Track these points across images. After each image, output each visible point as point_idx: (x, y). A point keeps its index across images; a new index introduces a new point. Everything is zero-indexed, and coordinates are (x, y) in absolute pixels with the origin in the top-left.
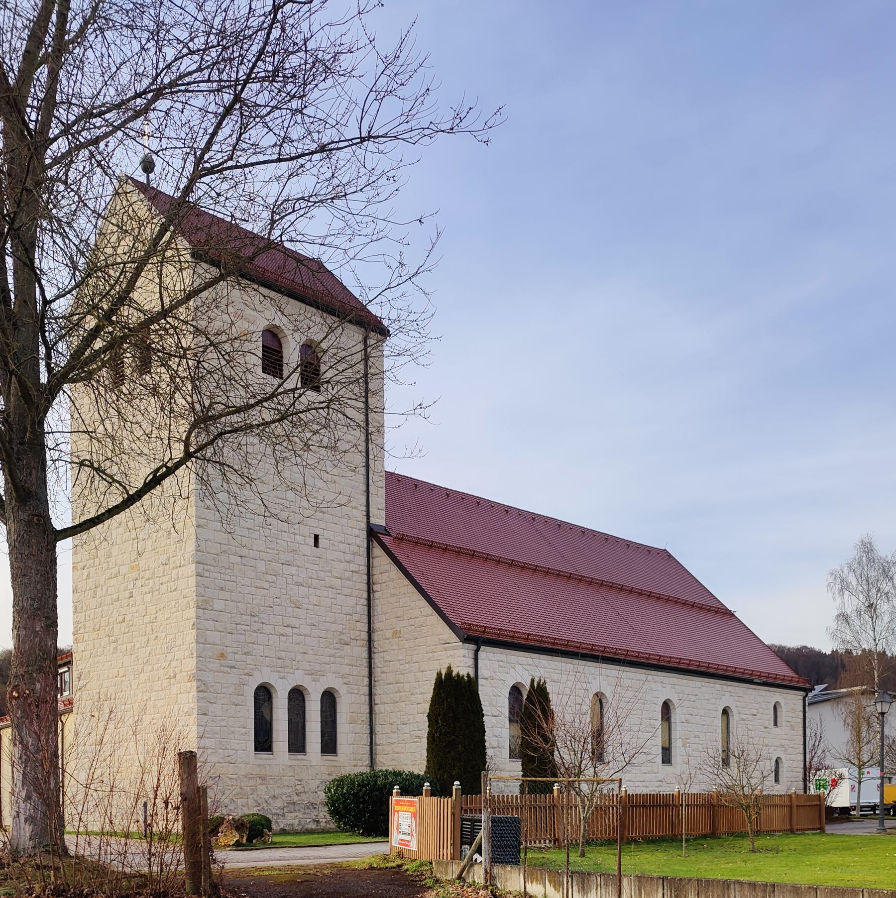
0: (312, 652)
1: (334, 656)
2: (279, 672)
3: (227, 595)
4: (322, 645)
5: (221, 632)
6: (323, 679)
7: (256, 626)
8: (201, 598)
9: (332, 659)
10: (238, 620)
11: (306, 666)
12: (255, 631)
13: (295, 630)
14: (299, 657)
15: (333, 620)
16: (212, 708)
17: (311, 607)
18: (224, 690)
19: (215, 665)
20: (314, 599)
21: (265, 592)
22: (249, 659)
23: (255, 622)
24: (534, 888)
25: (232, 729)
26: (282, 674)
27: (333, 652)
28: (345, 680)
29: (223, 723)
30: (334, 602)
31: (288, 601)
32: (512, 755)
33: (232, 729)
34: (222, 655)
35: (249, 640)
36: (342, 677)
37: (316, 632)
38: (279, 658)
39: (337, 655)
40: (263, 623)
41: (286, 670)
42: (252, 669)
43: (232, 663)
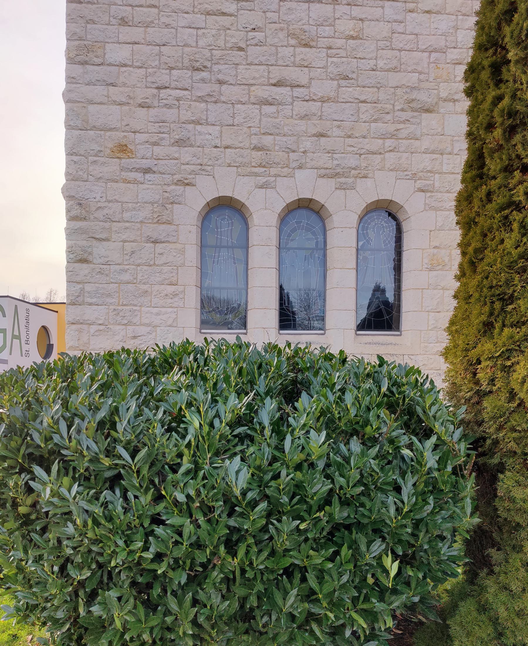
0: (336, 132)
1: (393, 136)
2: (256, 175)
3: (137, 33)
4: (364, 117)
5: (121, 104)
6: (202, 181)
7: (204, 89)
8: (77, 43)
9: (389, 143)
10: (163, 78)
11: (324, 160)
12: (201, 99)
13: (298, 92)
14: (307, 144)
15: (395, 63)
16: (100, 250)
17: (340, 42)
18: (127, 215)
19: (112, 167)
20: (346, 26)
21: (225, 21)
22: (186, 154)
23: (203, 80)
24: (4, 426)
25: (145, 287)
26: (262, 180)
27: (391, 128)
28: (419, 184)
29: (126, 277)
30: (400, 28)
31: (281, 35)
32: (455, 297)
33: (145, 287)
34: (122, 149)
35: (186, 115)
36: (414, 177)
37: (349, 92)
38: (256, 148)
39: (403, 134)
40: (221, 82)
41: (273, 171)
42: (192, 172)
43: (145, 163)
